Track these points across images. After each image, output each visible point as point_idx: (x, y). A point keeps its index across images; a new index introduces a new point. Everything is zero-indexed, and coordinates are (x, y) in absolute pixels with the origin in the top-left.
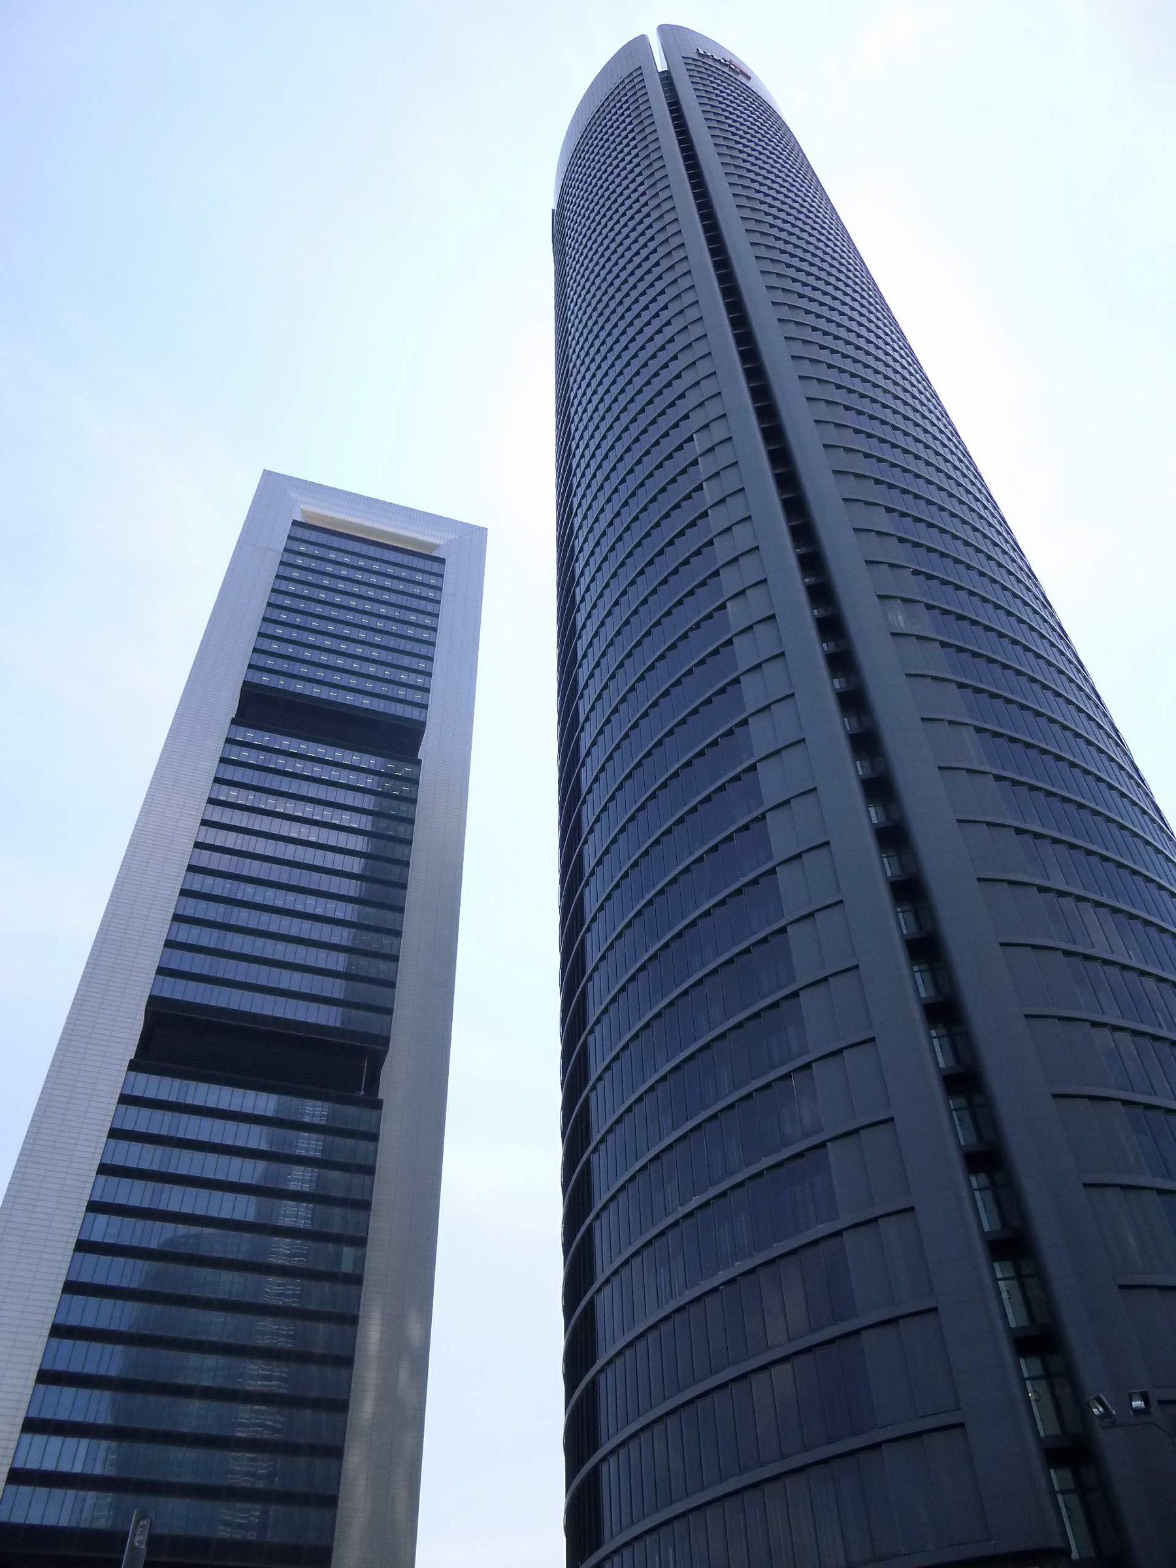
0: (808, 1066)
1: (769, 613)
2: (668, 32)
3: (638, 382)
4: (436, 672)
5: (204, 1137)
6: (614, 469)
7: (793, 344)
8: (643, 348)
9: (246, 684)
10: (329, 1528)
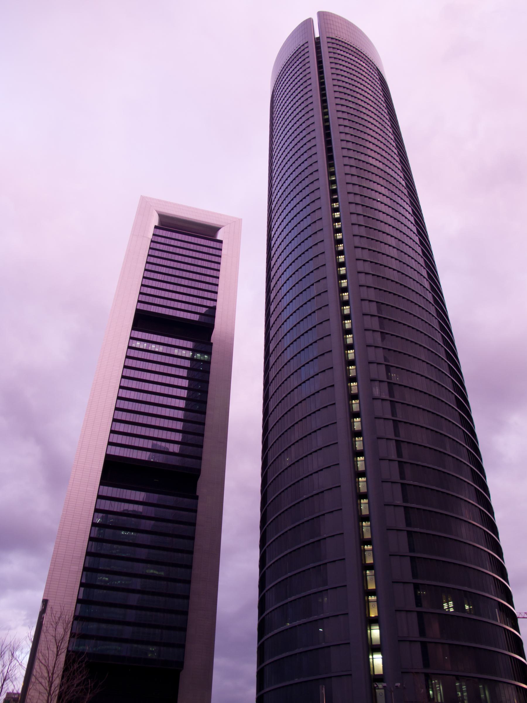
0: (326, 564)
1: (332, 384)
2: (322, 15)
3: (294, 78)
4: (219, 300)
5: (132, 498)
6: (284, 151)
7: (336, 93)
8: (297, 95)
9: (137, 310)
10: (204, 430)
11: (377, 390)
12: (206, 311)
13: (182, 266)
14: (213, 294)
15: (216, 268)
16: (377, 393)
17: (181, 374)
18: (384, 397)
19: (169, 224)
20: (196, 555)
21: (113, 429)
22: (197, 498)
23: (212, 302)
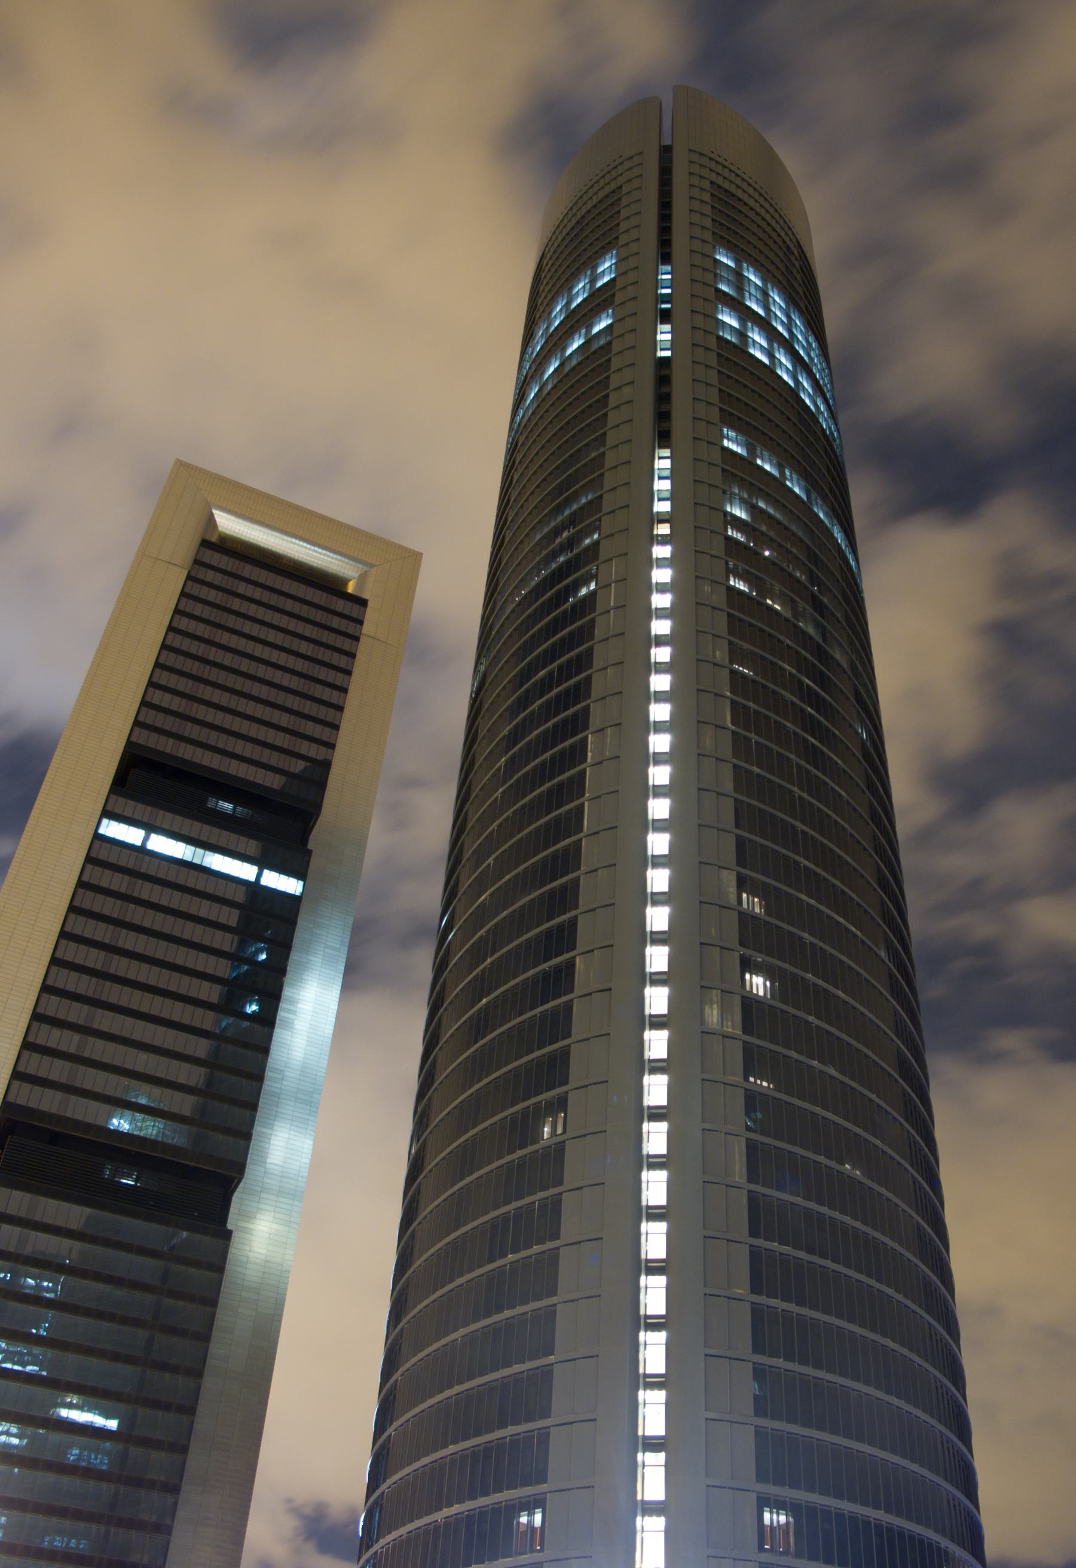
10: (251, 1125)
11: (715, 1012)
12: (306, 768)
13: (258, 650)
14: (331, 711)
15: (334, 701)
16: (715, 1020)
17: (223, 920)
18: (731, 1079)
19: (223, 571)
20: (209, 1383)
21: (49, 982)
22: (227, 1235)
23: (323, 749)
